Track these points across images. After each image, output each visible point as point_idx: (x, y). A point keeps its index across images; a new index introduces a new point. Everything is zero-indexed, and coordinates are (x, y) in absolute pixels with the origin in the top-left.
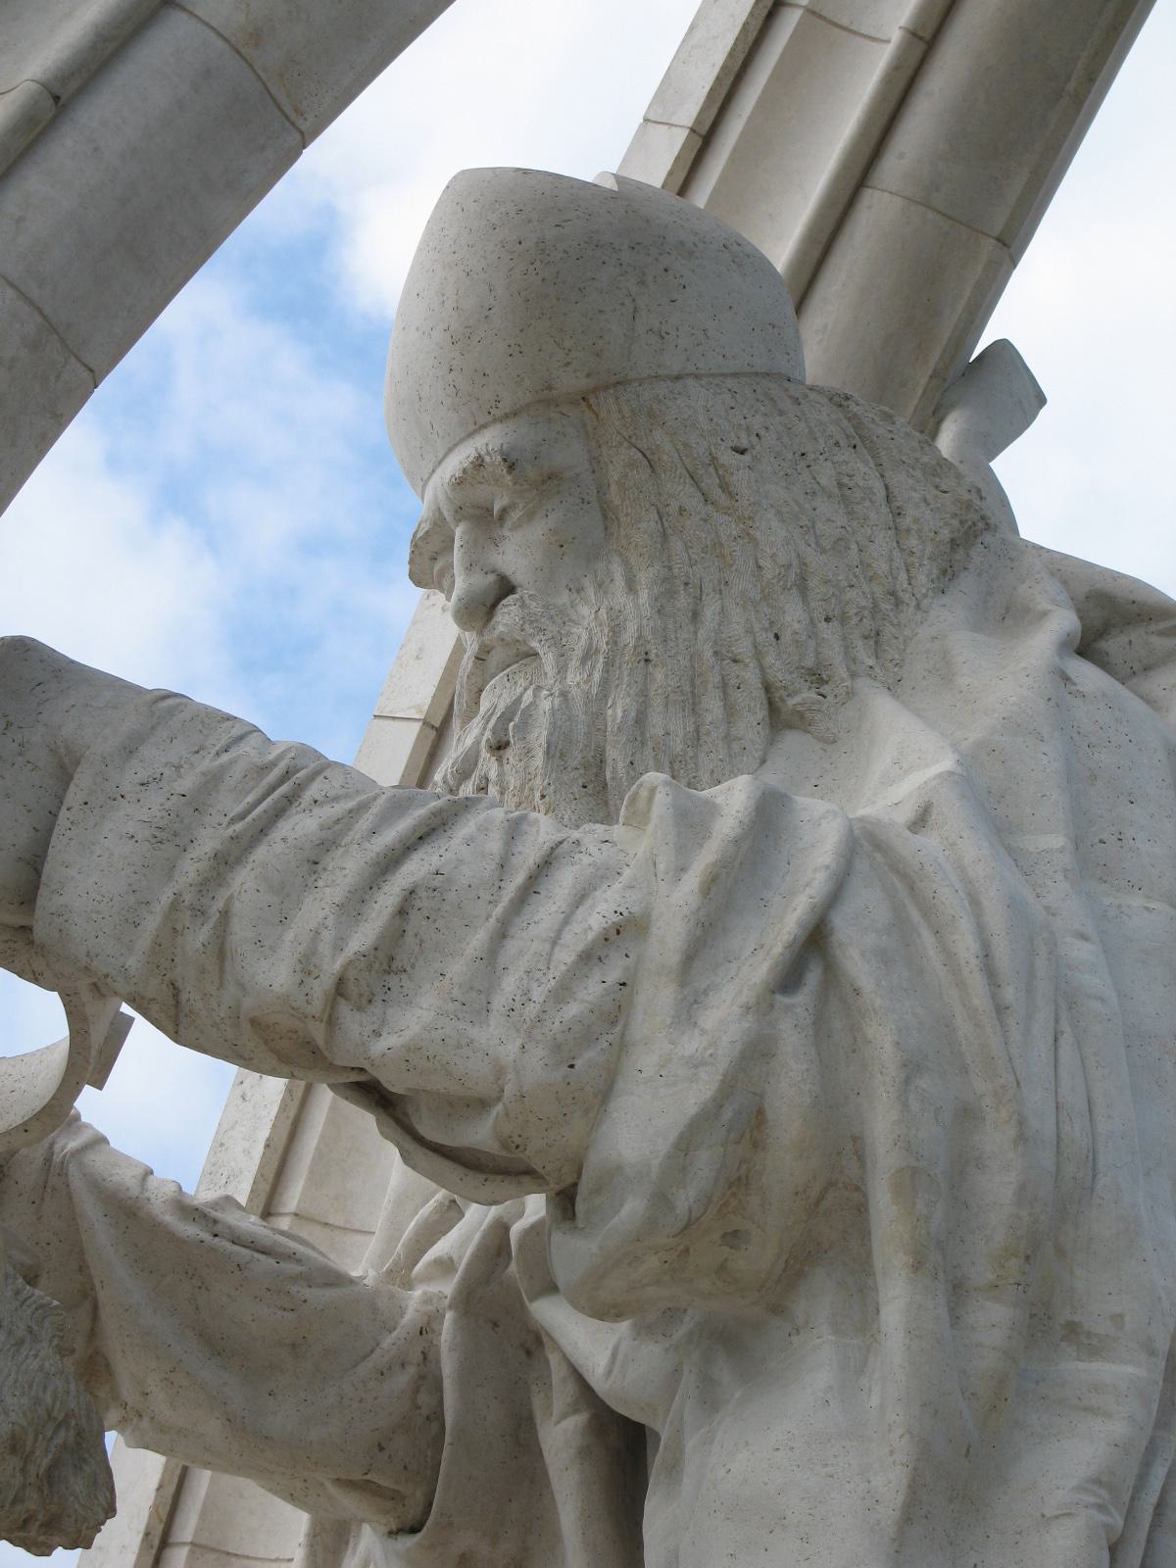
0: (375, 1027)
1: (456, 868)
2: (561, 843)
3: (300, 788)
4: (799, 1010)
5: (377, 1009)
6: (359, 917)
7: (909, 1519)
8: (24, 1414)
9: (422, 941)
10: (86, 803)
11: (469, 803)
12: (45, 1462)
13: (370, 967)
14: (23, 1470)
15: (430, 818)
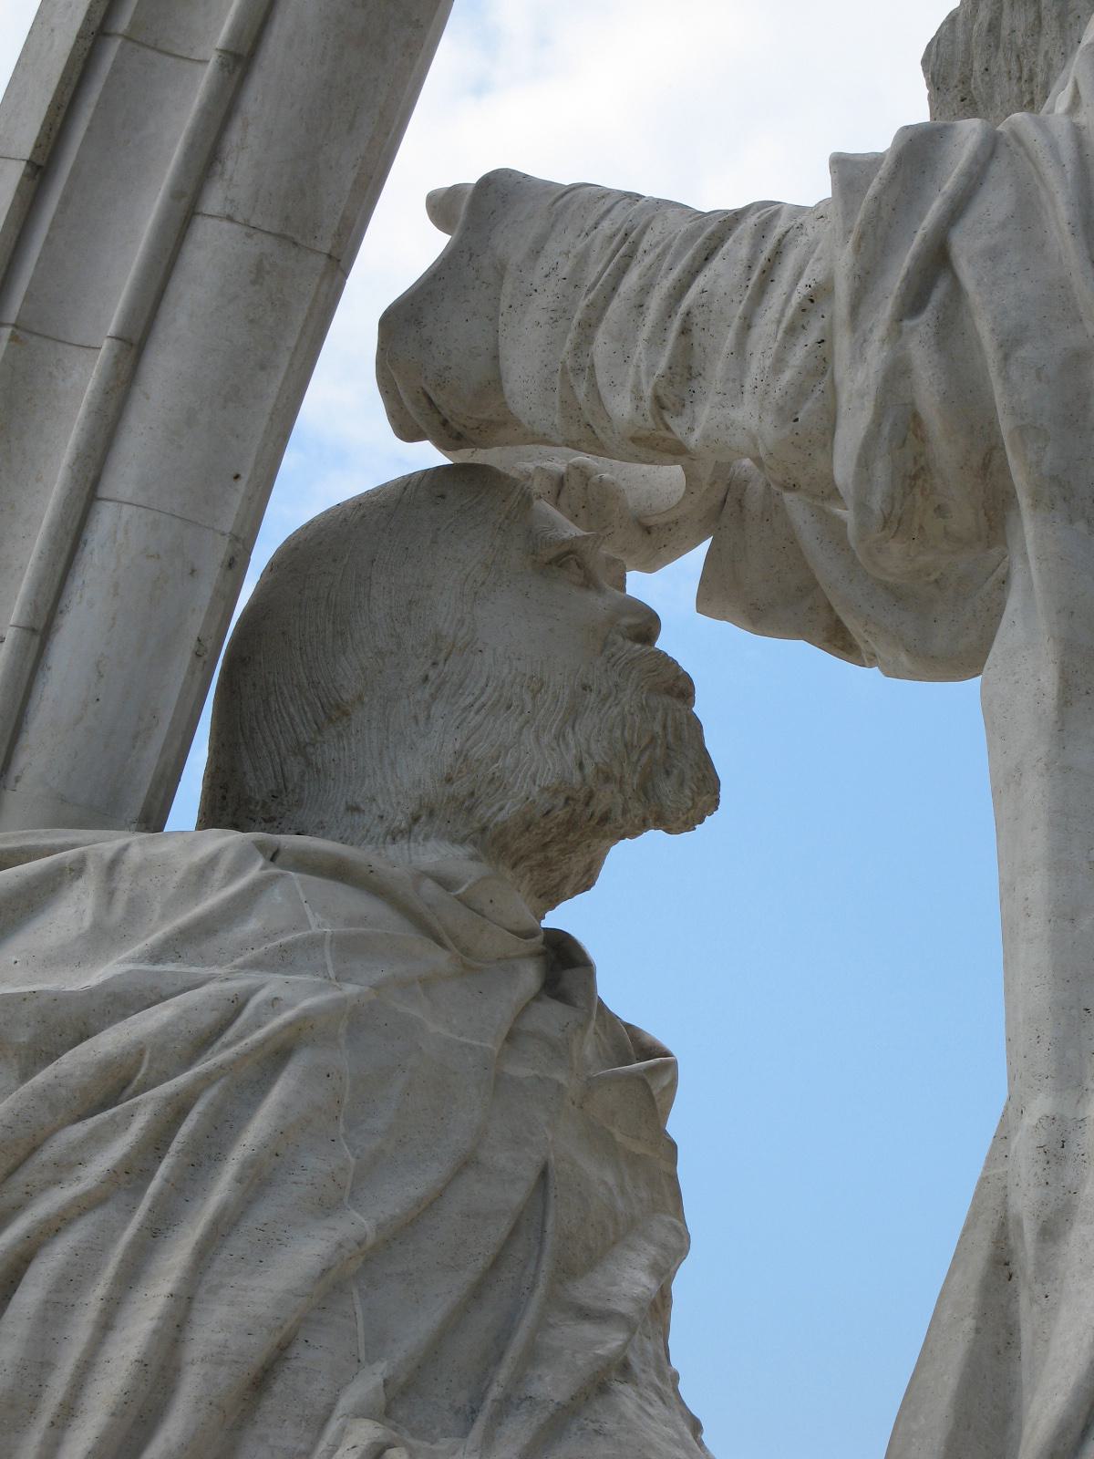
0: (688, 425)
1: (715, 282)
2: (787, 232)
3: (636, 244)
4: (921, 328)
5: (687, 411)
6: (665, 343)
7: (1066, 702)
8: (606, 753)
9: (704, 349)
10: (511, 307)
11: (739, 217)
12: (636, 780)
13: (671, 383)
14: (621, 791)
15: (705, 243)
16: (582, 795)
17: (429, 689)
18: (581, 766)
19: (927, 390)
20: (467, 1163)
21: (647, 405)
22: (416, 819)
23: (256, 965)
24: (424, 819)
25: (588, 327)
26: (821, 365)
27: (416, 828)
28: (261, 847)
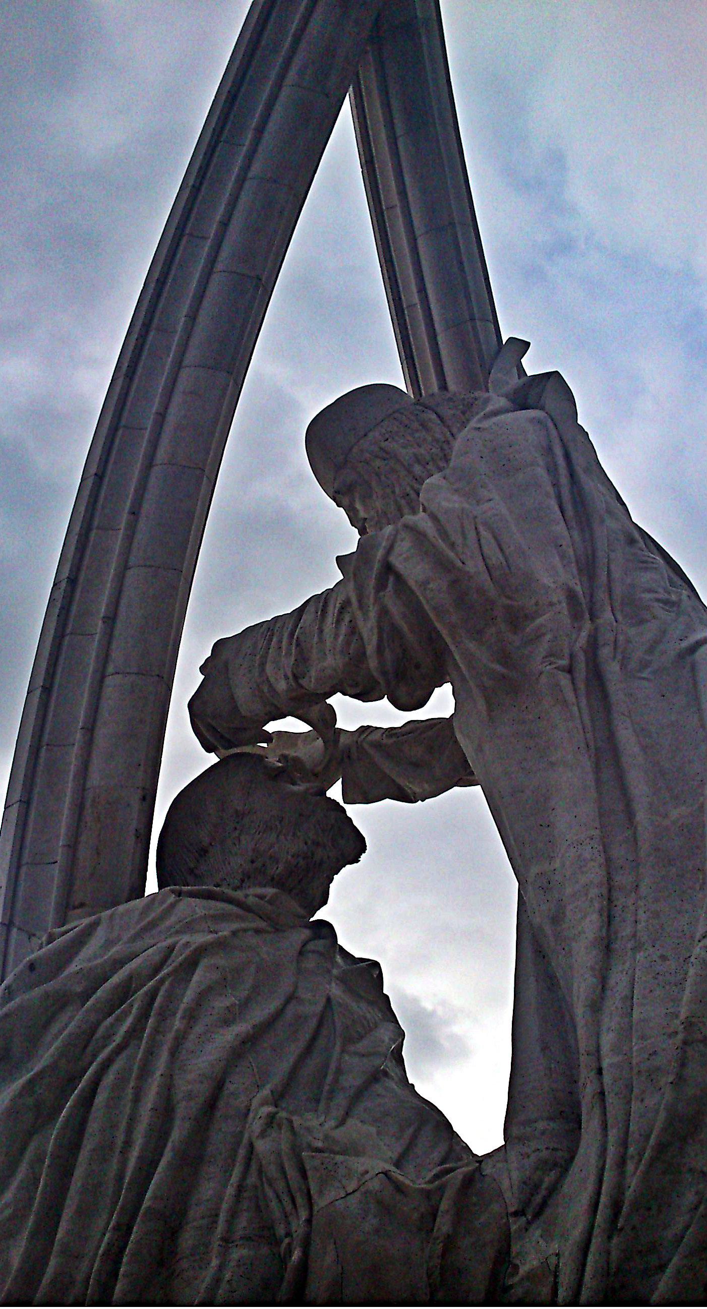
16: (309, 854)
17: (237, 832)
18: (306, 843)
19: (396, 609)
20: (291, 998)
21: (291, 681)
22: (242, 881)
23: (177, 932)
24: (246, 880)
25: (263, 665)
26: (353, 630)
27: (244, 885)
28: (173, 891)
